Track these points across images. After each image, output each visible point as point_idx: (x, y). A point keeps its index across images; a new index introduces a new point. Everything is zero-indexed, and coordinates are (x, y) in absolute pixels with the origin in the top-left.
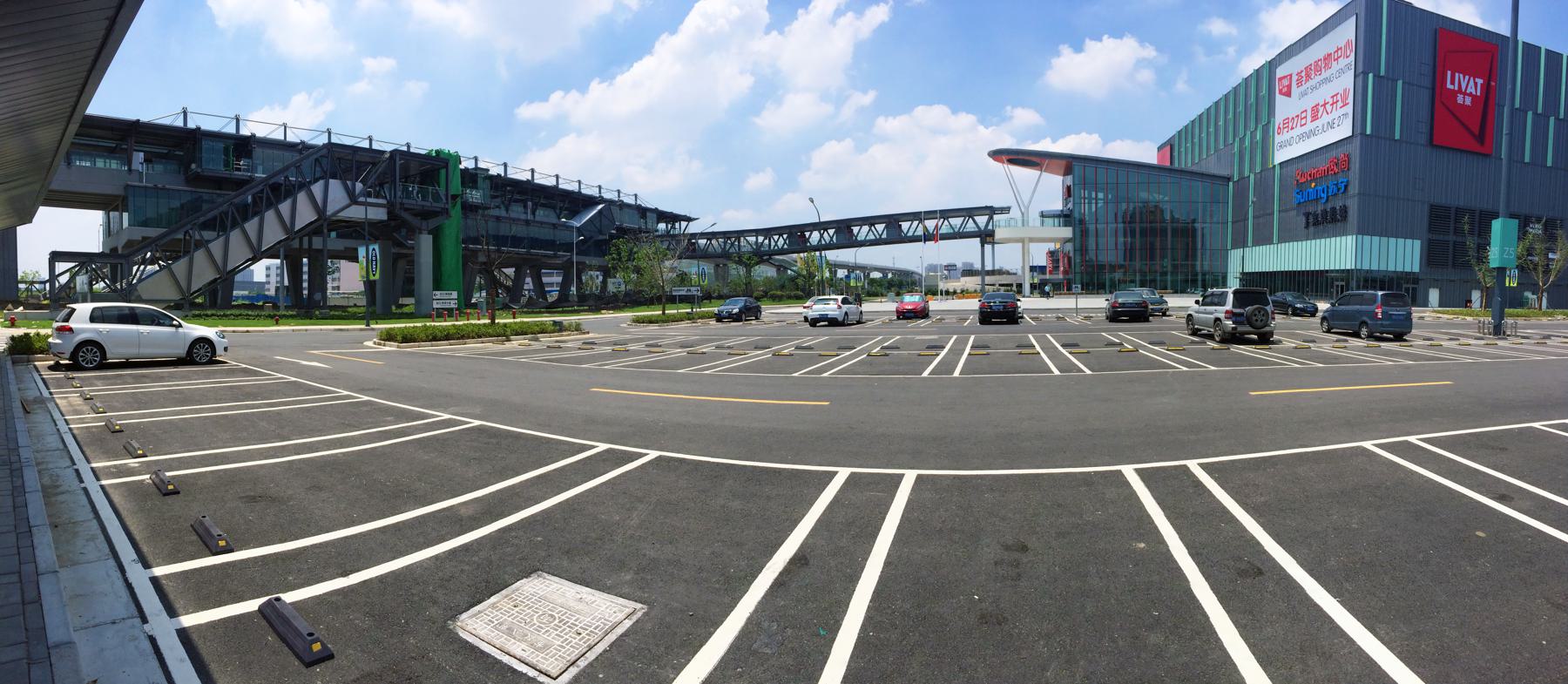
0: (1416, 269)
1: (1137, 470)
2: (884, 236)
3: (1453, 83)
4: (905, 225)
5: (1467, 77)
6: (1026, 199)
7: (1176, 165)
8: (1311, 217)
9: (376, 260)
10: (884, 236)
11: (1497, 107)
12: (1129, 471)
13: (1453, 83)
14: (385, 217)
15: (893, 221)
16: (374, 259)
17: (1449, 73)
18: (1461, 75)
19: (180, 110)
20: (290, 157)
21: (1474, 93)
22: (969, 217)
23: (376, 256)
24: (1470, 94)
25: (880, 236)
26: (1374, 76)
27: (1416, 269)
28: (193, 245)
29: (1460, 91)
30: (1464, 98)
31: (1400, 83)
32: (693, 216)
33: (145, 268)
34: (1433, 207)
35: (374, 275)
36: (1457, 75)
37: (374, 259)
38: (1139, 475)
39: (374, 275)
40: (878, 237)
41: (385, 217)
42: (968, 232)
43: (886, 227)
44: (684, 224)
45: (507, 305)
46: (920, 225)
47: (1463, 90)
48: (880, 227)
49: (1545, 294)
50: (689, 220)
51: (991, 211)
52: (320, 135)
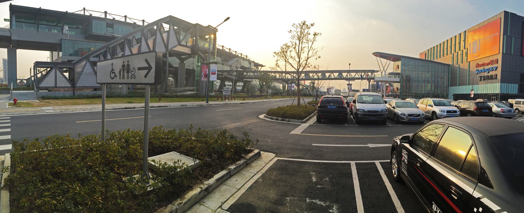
0: (517, 93)
1: (380, 163)
2: (304, 78)
4: (311, 75)
7: (427, 59)
8: (482, 78)
10: (304, 78)
11: (105, 35)
12: (377, 163)
15: (340, 72)
19: (82, 9)
20: (132, 30)
22: (332, 73)
25: (303, 77)
26: (506, 36)
27: (517, 93)
31: (513, 38)
32: (264, 65)
34: (363, 89)
38: (381, 165)
40: (302, 78)
42: (356, 78)
43: (304, 75)
44: (260, 67)
46: (316, 75)
48: (320, 74)
49: (27, 206)
50: (262, 66)
51: (373, 72)
52: (139, 22)
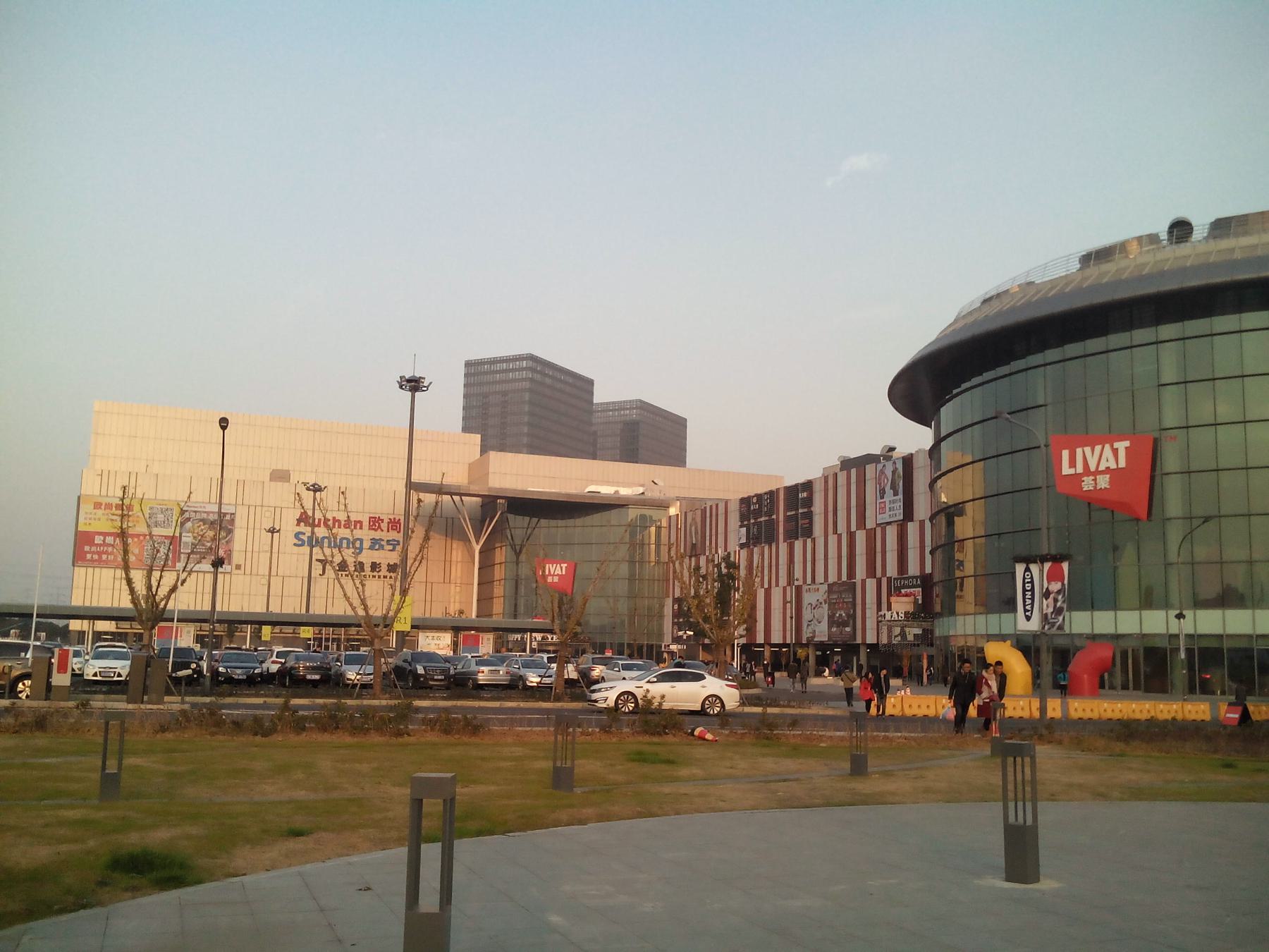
3: (1073, 463)
5: (555, 565)
6: (1203, 520)
9: (1032, 590)
13: (1073, 463)
14: (855, 469)
16: (1028, 587)
17: (1065, 453)
18: (551, 565)
21: (1113, 466)
23: (1032, 582)
24: (558, 575)
28: (1093, 257)
29: (1087, 471)
30: (1095, 480)
33: (365, 668)
35: (1028, 618)
36: (1079, 451)
37: (1028, 587)
39: (1028, 618)
41: (855, 469)
45: (1038, 650)
47: (552, 573)
